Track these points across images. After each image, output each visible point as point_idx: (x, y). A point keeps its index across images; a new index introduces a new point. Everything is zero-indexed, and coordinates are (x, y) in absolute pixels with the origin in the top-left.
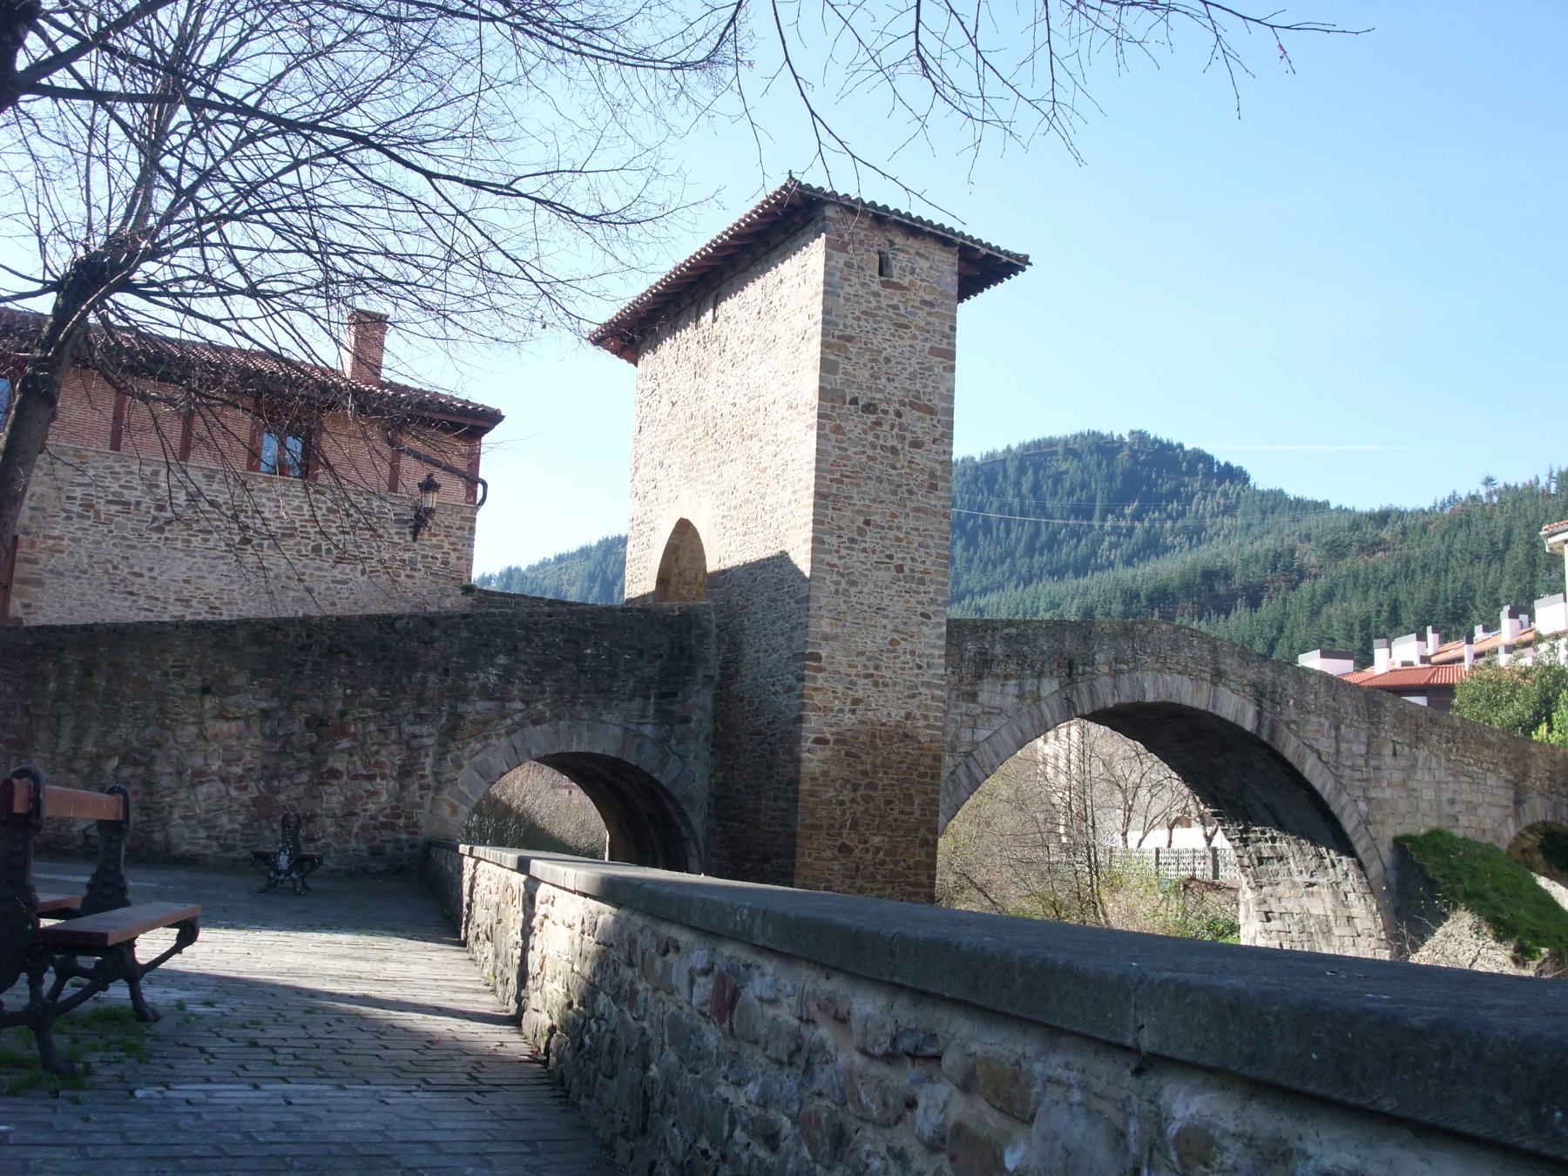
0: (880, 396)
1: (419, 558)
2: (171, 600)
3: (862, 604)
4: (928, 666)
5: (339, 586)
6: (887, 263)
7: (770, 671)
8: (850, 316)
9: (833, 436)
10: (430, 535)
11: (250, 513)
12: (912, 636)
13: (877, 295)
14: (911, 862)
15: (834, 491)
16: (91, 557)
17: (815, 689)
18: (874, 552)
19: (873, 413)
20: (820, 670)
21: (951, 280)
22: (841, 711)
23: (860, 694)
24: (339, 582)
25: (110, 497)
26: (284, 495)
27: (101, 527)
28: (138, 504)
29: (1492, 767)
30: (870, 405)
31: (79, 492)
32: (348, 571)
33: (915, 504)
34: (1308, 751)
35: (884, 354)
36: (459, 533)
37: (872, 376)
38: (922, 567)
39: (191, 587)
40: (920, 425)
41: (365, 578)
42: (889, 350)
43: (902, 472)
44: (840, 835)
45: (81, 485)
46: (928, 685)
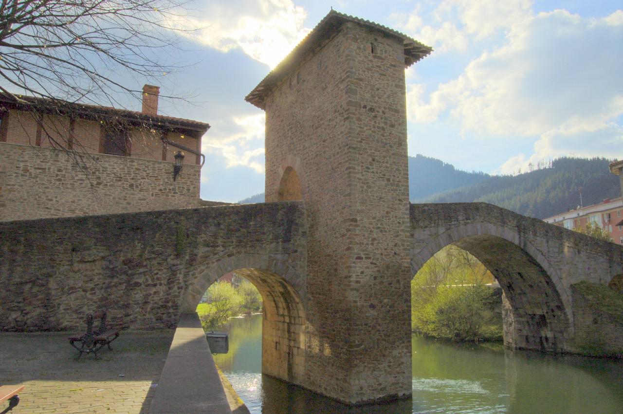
0: (375, 104)
1: (177, 188)
2: (66, 211)
3: (373, 196)
4: (403, 223)
5: (142, 201)
6: (375, 48)
7: (333, 228)
8: (361, 70)
9: (356, 122)
10: (181, 178)
11: (101, 172)
12: (395, 210)
13: (371, 61)
14: (400, 309)
15: (359, 146)
16: (28, 193)
17: (356, 235)
18: (377, 173)
19: (372, 112)
20: (358, 226)
21: (402, 57)
22: (367, 244)
23: (375, 236)
24: (142, 200)
25: (37, 167)
26: (116, 163)
27: (32, 180)
28: (49, 169)
29: (601, 254)
30: (371, 108)
31: (22, 165)
32: (146, 195)
33: (393, 152)
34: (538, 252)
35: (376, 86)
36: (194, 177)
37: (372, 96)
38: (398, 180)
39: (75, 205)
40: (393, 117)
41: (154, 197)
42: (378, 85)
43: (387, 138)
44: (370, 300)
45: (22, 161)
46: (402, 230)
